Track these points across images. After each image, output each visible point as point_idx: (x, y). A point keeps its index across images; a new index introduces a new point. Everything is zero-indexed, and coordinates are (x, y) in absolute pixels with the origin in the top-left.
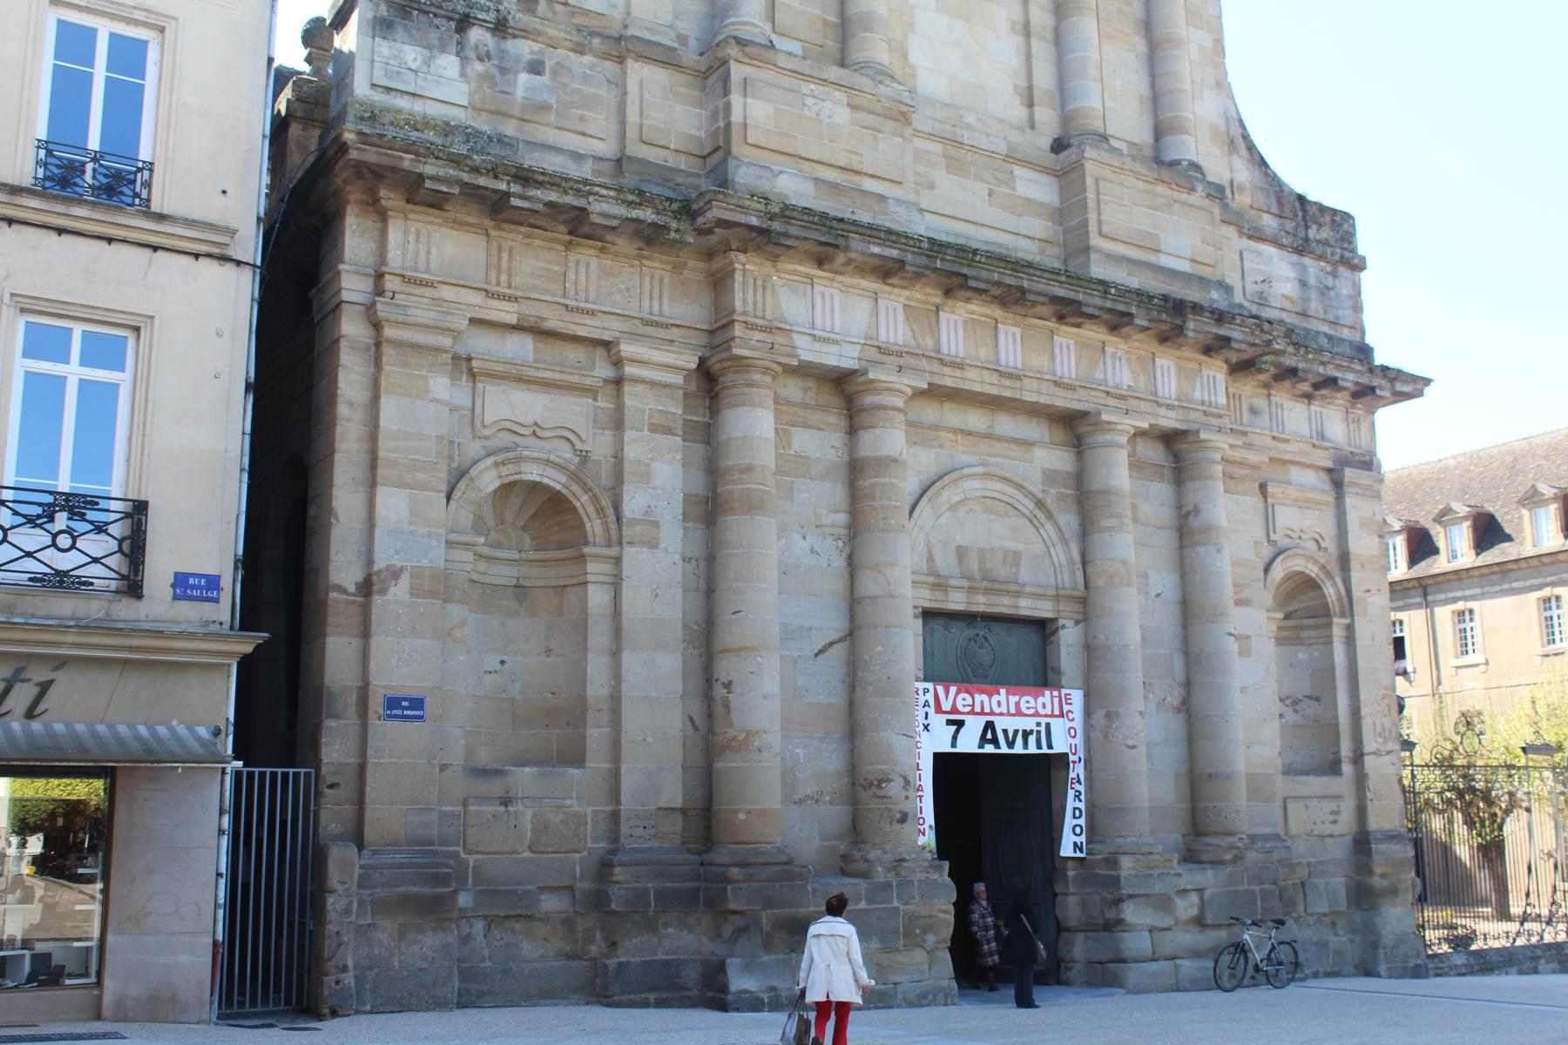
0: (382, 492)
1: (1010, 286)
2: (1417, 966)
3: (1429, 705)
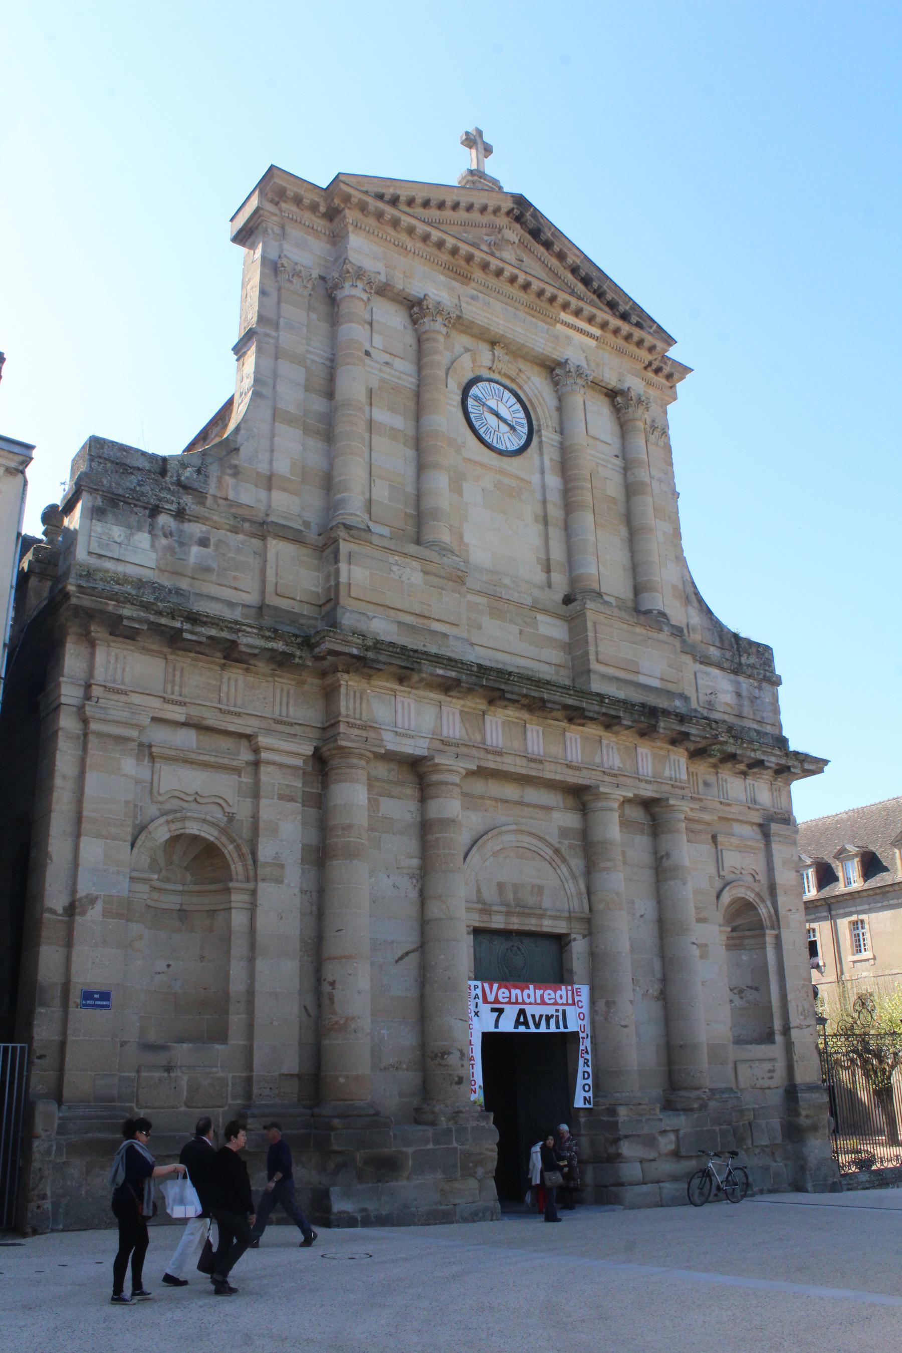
0: (84, 841)
1: (534, 697)
2: (834, 1183)
3: (835, 989)
